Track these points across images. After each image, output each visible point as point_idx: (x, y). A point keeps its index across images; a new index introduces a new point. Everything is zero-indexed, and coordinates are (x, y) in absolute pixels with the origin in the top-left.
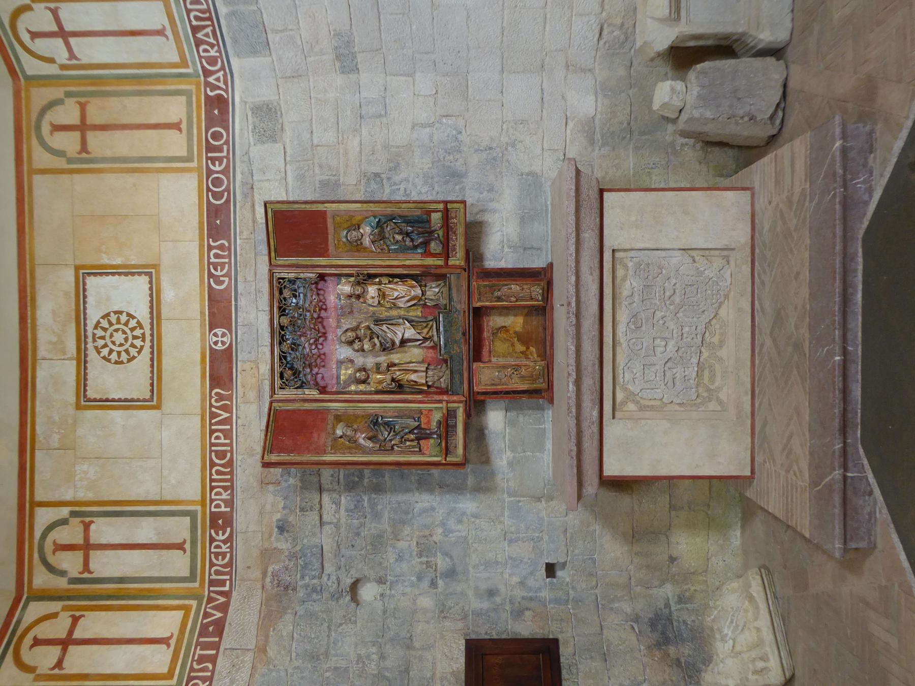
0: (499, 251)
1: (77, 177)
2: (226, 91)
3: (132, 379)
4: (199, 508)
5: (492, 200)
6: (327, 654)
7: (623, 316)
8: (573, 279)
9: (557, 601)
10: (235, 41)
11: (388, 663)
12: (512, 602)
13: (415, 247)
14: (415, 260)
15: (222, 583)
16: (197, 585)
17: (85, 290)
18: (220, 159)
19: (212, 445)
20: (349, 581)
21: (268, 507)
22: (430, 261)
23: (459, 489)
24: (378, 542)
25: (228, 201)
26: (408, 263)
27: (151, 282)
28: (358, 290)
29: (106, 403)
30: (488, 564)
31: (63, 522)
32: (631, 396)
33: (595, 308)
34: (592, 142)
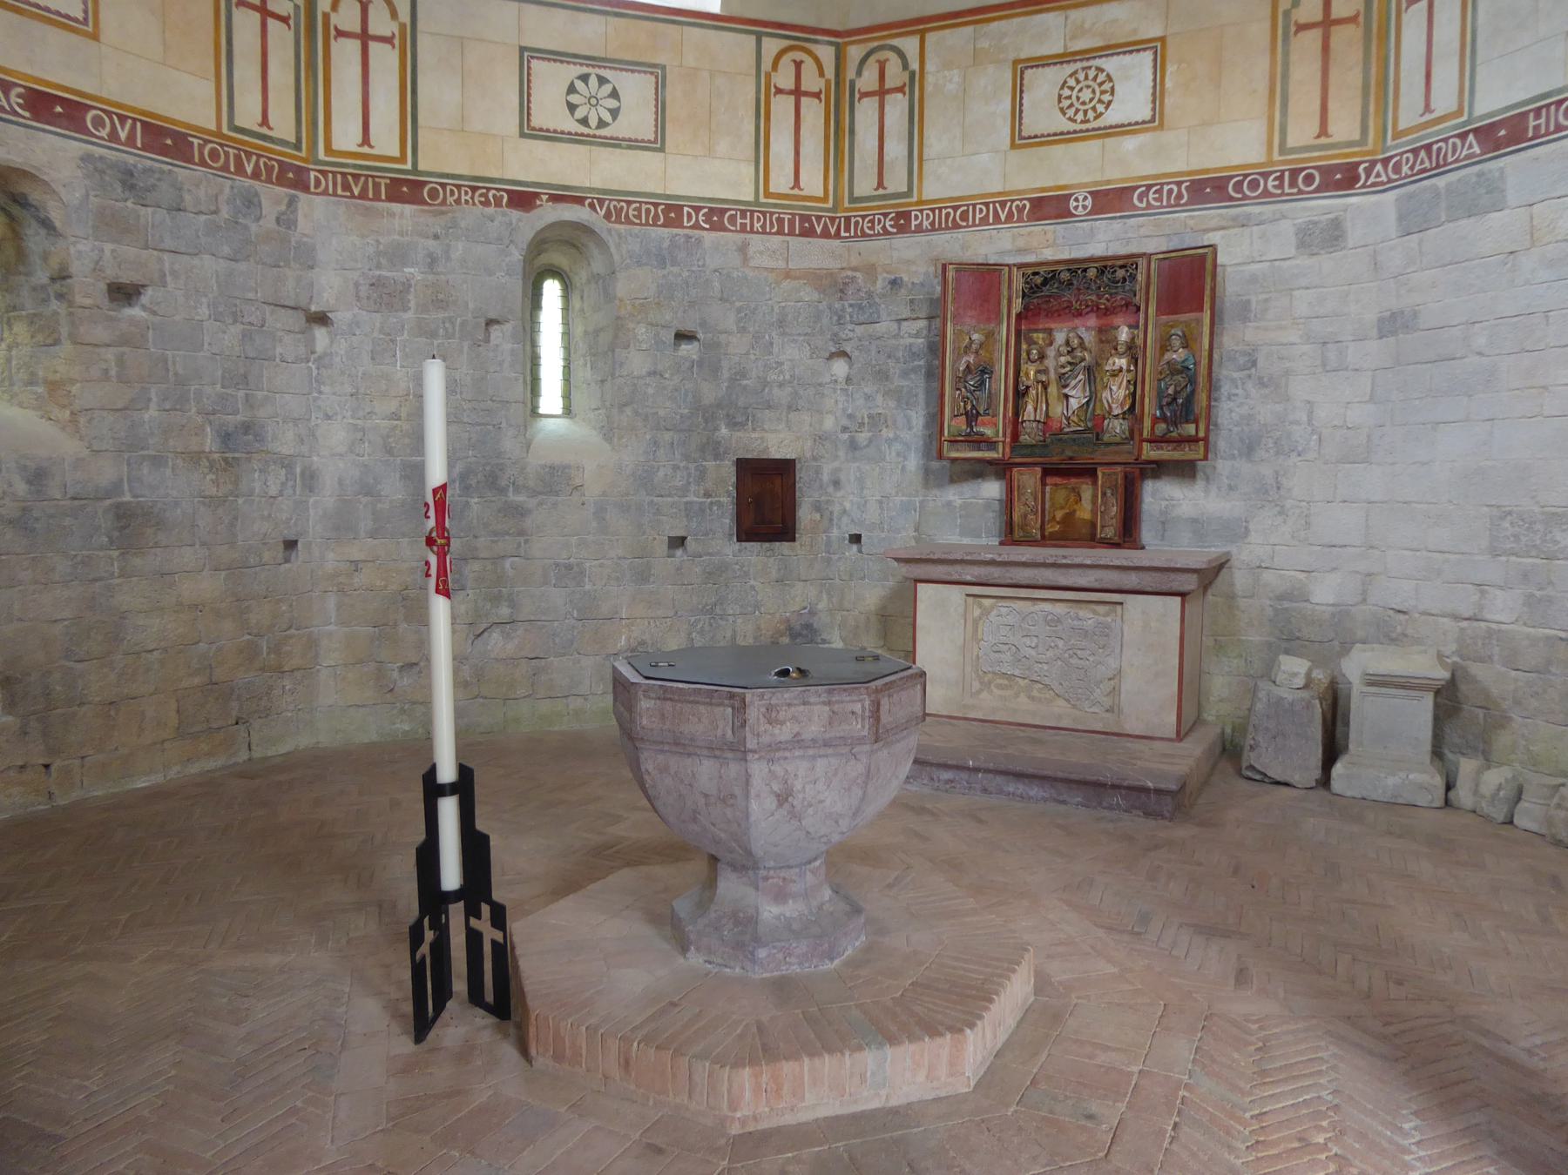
0: (1158, 496)
1: (1267, 25)
2: (1364, 186)
3: (1043, 115)
4: (915, 199)
5: (1219, 488)
6: (784, 334)
7: (1060, 609)
8: (1088, 562)
9: (828, 543)
10: (1411, 196)
11: (776, 391)
12: (828, 502)
13: (1161, 408)
14: (1149, 407)
15: (847, 229)
16: (846, 205)
17: (1138, 51)
18: (1281, 186)
19: (974, 206)
20: (848, 350)
21: (913, 268)
22: (1147, 423)
23: (926, 454)
24: (882, 376)
25: (1231, 199)
26: (1147, 400)
27: (1144, 122)
28: (1121, 349)
29: (1018, 91)
30: (861, 481)
31: (905, 66)
32: (986, 612)
33: (1063, 581)
34: (1281, 598)
